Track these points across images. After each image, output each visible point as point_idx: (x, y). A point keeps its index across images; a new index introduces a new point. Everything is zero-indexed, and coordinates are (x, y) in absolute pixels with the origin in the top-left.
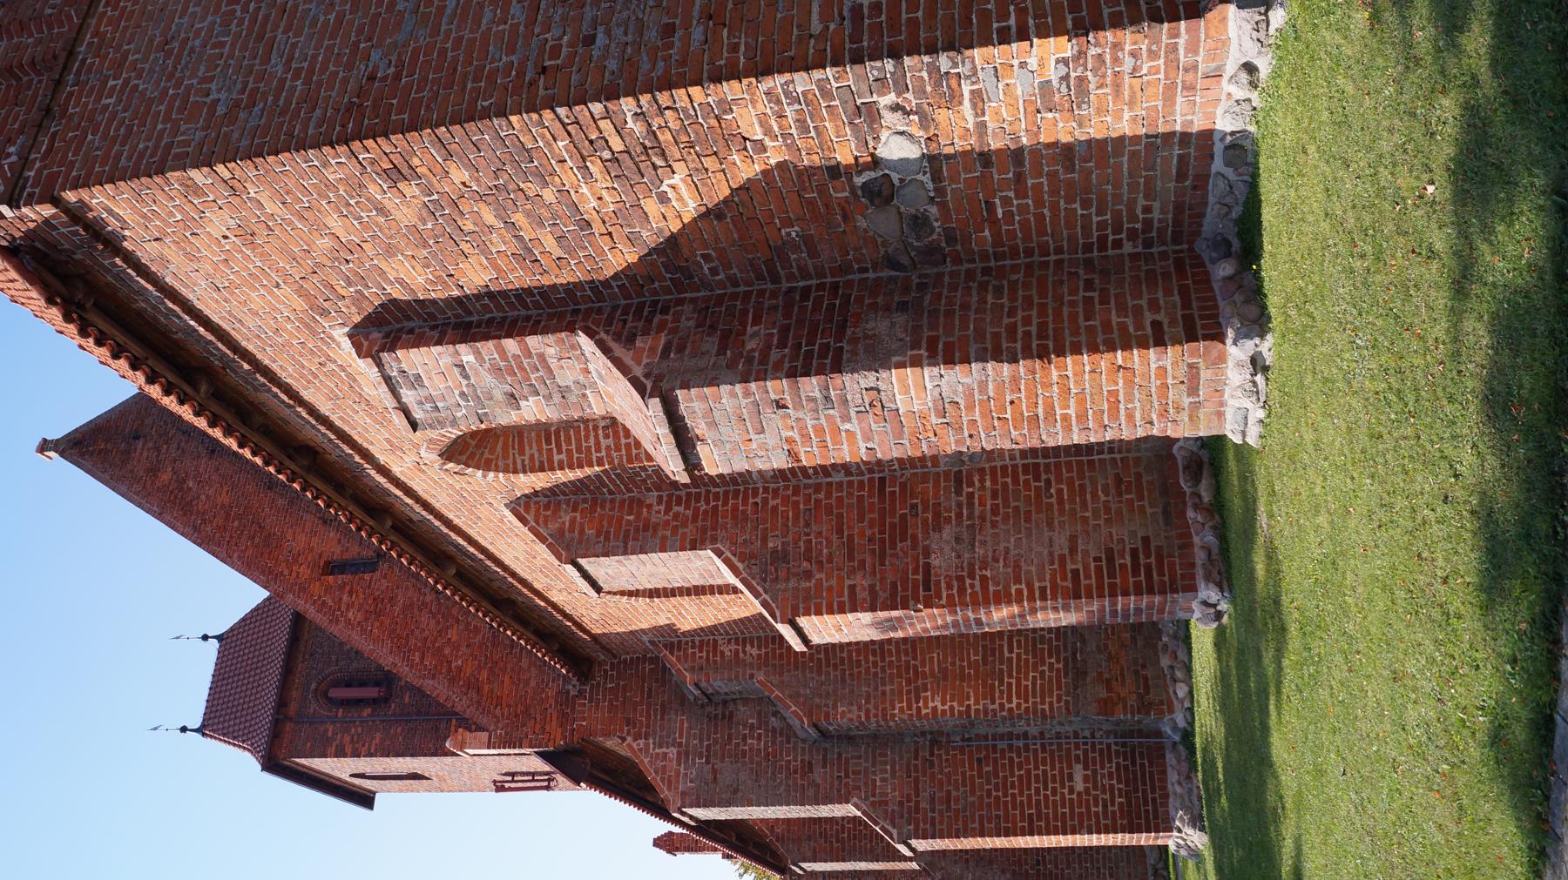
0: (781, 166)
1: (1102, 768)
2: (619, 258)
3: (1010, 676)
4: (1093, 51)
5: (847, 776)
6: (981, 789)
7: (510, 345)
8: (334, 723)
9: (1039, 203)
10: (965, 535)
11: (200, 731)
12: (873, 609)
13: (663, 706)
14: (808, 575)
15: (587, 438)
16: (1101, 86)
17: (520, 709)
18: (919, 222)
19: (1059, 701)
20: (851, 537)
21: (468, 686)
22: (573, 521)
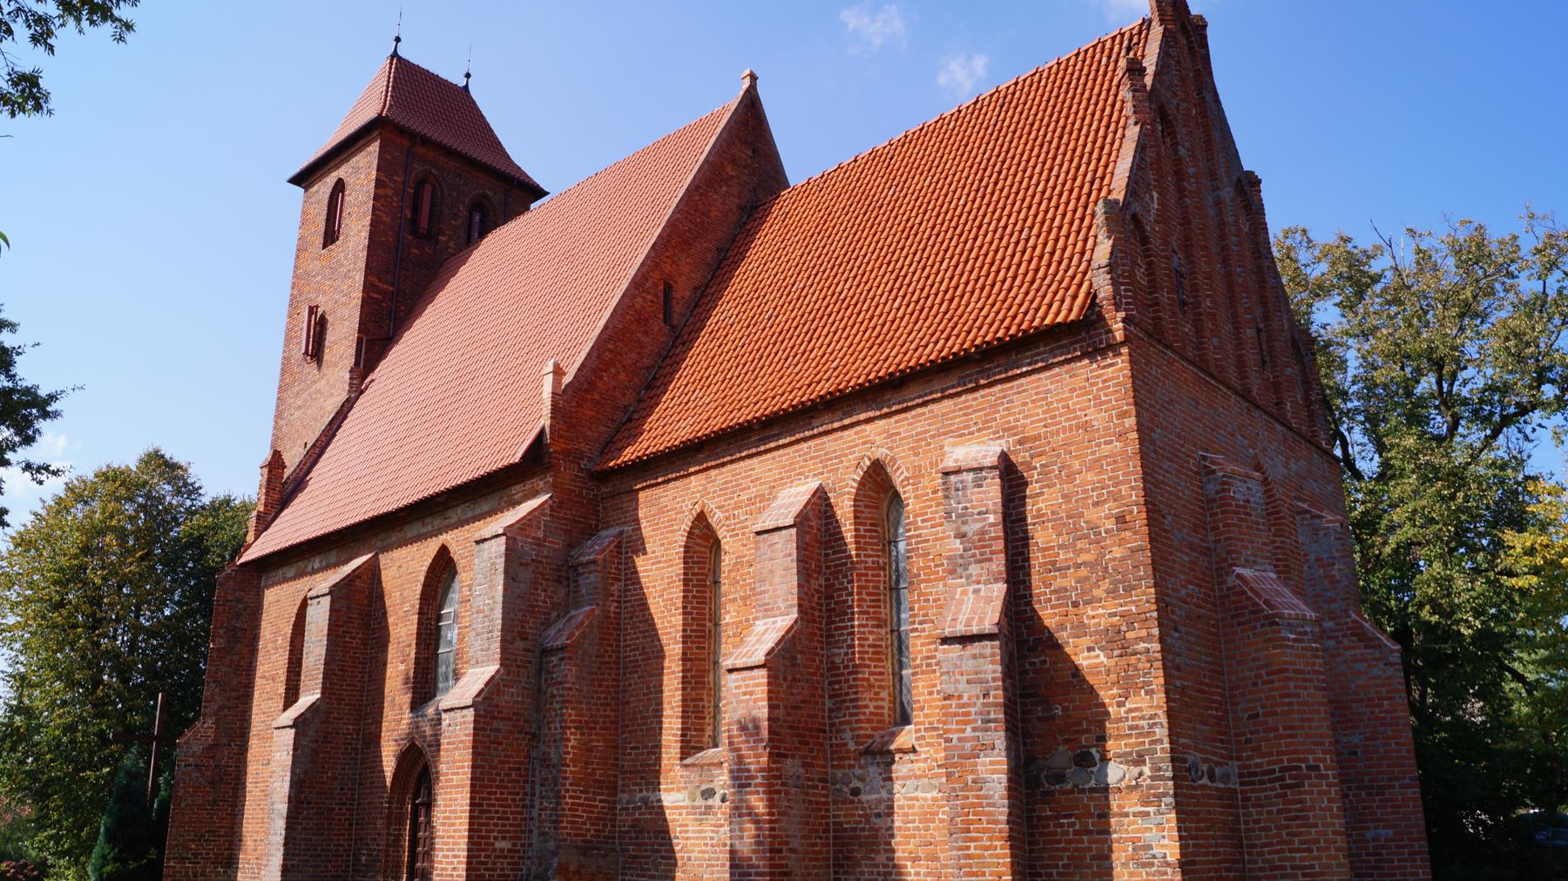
0: (1108, 713)
1: (508, 864)
2: (1050, 616)
3: (586, 799)
4: (1169, 870)
5: (518, 666)
6: (502, 769)
7: (1000, 545)
8: (404, 183)
9: (1069, 842)
10: (800, 782)
11: (395, 55)
12: (770, 719)
13: (570, 531)
14: (785, 679)
15: (873, 550)
16: (1148, 874)
17: (574, 421)
18: (1060, 778)
19: (568, 834)
20: (800, 708)
21: (591, 384)
22: (812, 527)
